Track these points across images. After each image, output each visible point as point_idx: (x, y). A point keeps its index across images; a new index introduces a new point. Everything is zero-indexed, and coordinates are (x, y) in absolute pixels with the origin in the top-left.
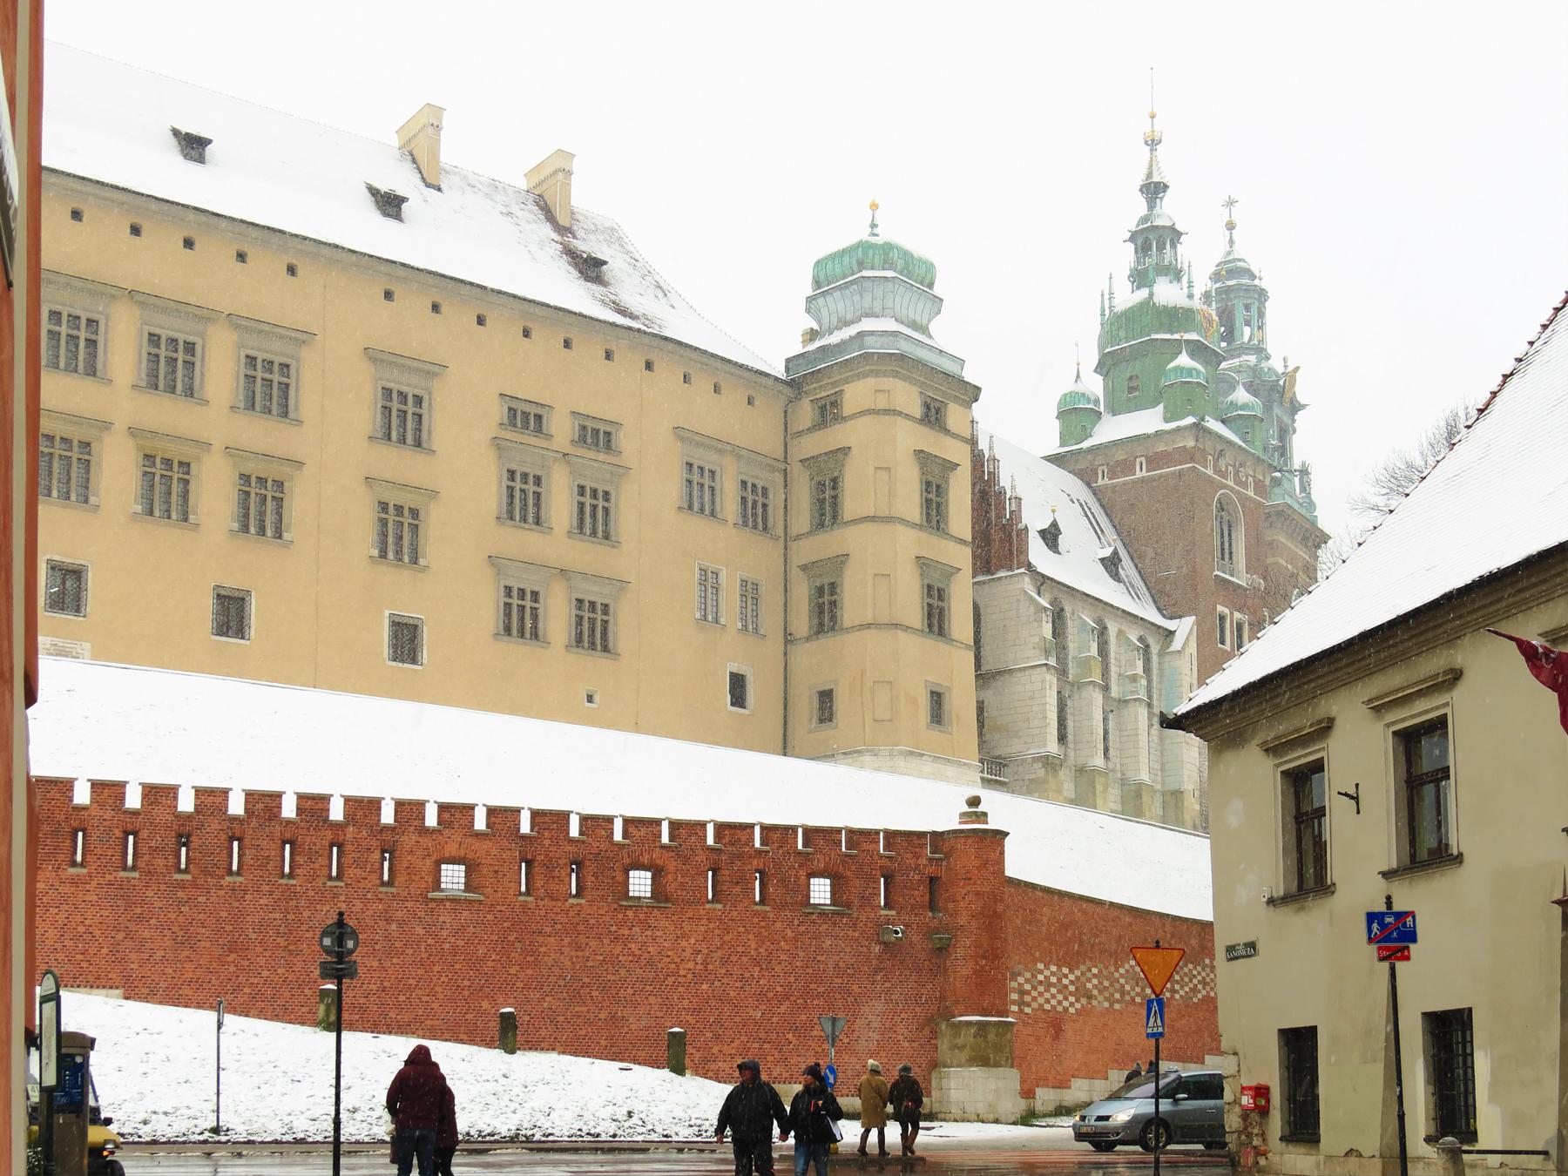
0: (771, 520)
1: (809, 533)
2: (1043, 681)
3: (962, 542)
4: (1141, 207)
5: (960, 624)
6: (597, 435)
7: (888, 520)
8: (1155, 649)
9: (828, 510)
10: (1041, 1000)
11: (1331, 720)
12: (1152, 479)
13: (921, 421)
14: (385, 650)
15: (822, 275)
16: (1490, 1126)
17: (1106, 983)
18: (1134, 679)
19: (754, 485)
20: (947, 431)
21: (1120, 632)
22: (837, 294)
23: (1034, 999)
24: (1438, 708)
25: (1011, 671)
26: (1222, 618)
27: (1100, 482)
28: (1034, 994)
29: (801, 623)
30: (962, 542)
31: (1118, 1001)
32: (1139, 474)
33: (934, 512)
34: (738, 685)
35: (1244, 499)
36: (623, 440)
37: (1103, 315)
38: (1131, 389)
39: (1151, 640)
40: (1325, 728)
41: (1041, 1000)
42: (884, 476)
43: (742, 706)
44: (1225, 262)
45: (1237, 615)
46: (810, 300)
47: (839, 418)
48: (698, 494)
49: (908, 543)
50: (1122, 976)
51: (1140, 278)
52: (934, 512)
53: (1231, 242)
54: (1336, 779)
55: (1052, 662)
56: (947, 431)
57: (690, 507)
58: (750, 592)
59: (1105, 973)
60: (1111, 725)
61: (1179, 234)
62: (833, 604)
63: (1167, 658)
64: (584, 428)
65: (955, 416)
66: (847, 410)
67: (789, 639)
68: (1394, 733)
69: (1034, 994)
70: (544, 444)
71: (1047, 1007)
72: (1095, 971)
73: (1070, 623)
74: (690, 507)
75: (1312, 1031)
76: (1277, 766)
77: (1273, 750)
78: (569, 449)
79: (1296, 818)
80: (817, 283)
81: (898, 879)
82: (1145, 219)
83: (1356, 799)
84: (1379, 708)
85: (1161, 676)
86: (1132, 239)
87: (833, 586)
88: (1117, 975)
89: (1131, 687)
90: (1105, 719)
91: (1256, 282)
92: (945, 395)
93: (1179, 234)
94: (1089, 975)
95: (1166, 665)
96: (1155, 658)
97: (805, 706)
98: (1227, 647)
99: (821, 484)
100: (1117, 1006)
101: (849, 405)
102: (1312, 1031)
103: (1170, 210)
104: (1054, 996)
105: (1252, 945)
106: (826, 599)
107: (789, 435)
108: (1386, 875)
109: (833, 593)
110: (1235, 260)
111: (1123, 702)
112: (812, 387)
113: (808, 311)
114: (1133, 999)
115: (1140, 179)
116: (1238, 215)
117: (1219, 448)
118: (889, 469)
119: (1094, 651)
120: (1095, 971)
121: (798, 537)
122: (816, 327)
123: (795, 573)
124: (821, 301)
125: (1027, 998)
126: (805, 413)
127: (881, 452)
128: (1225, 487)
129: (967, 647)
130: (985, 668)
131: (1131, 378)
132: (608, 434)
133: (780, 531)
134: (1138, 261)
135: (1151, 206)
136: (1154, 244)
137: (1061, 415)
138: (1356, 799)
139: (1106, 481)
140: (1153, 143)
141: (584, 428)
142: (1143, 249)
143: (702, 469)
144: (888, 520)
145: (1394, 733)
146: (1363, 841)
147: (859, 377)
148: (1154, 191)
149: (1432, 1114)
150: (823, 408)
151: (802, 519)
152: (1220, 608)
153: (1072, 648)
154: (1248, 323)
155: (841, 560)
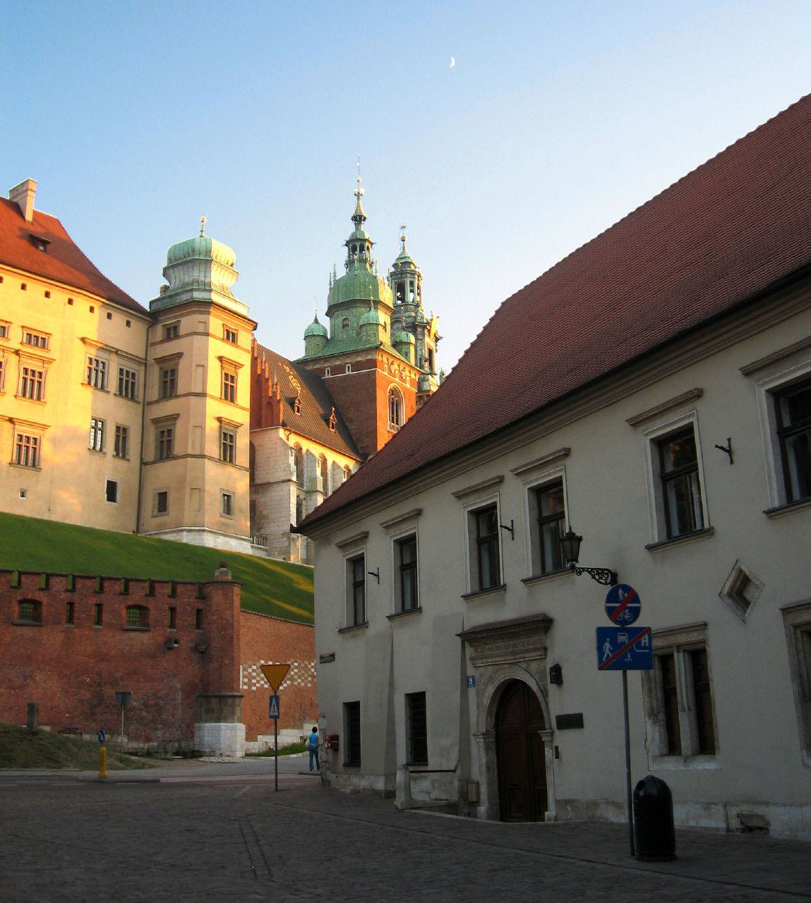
0: (136, 393)
1: (157, 402)
3: (243, 409)
5: (242, 457)
6: (37, 339)
9: (169, 387)
11: (368, 533)
12: (354, 376)
14: (325, 313)
15: (172, 254)
16: (433, 761)
19: (127, 372)
20: (238, 347)
22: (180, 267)
24: (411, 529)
25: (269, 484)
27: (327, 376)
29: (151, 455)
30: (243, 409)
32: (347, 373)
34: (112, 489)
35: (404, 388)
36: (53, 343)
37: (330, 284)
40: (365, 537)
42: (201, 368)
43: (114, 501)
44: (401, 259)
46: (165, 269)
47: (177, 337)
48: (96, 376)
50: (313, 667)
51: (350, 264)
53: (404, 248)
54: (370, 565)
57: (89, 383)
58: (122, 432)
59: (302, 665)
62: (169, 441)
64: (29, 335)
66: (182, 331)
67: (143, 463)
68: (395, 541)
70: (6, 344)
72: (296, 664)
74: (89, 383)
75: (358, 703)
76: (344, 556)
77: (343, 546)
78: (18, 347)
79: (354, 585)
80: (170, 260)
81: (178, 610)
82: (353, 234)
83: (377, 576)
84: (387, 527)
87: (169, 431)
88: (309, 666)
91: (417, 270)
97: (150, 502)
99: (166, 372)
101: (183, 330)
102: (358, 703)
103: (367, 230)
105: (333, 655)
106: (165, 439)
107: (149, 345)
108: (390, 618)
109: (169, 435)
110: (405, 258)
113: (164, 275)
115: (353, 213)
116: (406, 233)
117: (390, 360)
118: (203, 366)
120: (296, 664)
122: (168, 284)
123: (148, 421)
124: (171, 271)
126: (159, 331)
128: (394, 382)
130: (258, 481)
131: (344, 320)
132: (44, 339)
133: (141, 399)
134: (349, 257)
138: (377, 576)
141: (29, 335)
142: (353, 249)
143: (97, 361)
145: (395, 541)
146: (382, 596)
147: (189, 314)
148: (358, 219)
149: (716, 742)
150: (169, 330)
151: (154, 393)
154: (412, 291)
155: (174, 418)
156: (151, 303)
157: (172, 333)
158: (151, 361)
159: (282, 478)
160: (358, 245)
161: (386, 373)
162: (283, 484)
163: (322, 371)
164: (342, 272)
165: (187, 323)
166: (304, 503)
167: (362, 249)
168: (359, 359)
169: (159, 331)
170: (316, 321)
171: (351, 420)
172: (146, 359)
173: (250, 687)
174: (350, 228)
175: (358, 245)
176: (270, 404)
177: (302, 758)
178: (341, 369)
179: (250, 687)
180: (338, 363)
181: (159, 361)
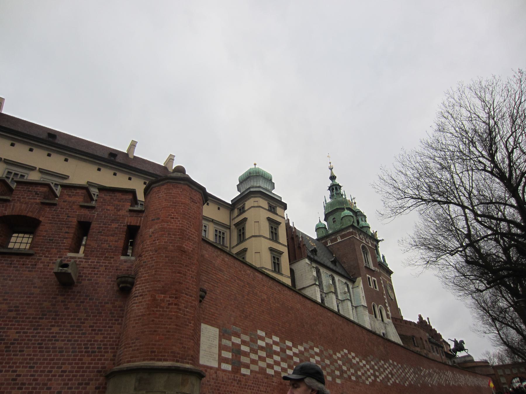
2: (315, 289)
4: (331, 182)
7: (260, 236)
8: (351, 286)
10: (262, 364)
13: (268, 210)
17: (327, 362)
18: (345, 293)
21: (339, 280)
23: (254, 362)
26: (369, 278)
27: (329, 245)
28: (253, 356)
31: (338, 377)
32: (339, 241)
33: (274, 236)
38: (334, 222)
39: (348, 283)
41: (262, 364)
42: (257, 224)
45: (373, 278)
46: (238, 186)
47: (244, 211)
49: (267, 244)
51: (332, 197)
52: (274, 236)
55: (317, 283)
56: (277, 214)
60: (340, 308)
61: (341, 187)
63: (355, 289)
65: (279, 210)
69: (253, 356)
71: (270, 372)
72: (317, 350)
73: (322, 275)
85: (354, 295)
86: (329, 189)
88: (335, 357)
89: (345, 296)
90: (338, 306)
92: (277, 204)
93: (341, 187)
94: (311, 352)
95: (355, 291)
96: (351, 289)
98: (372, 287)
99: (240, 230)
100: (338, 381)
103: (337, 181)
104: (277, 363)
111: (343, 301)
112: (238, 204)
114: (350, 377)
115: (329, 176)
119: (331, 282)
120: (317, 350)
121: (233, 247)
124: (241, 186)
125: (244, 360)
127: (257, 216)
129: (288, 277)
131: (334, 219)
133: (228, 245)
135: (332, 173)
136: (335, 188)
137: (316, 230)
139: (330, 244)
140: (331, 169)
144: (260, 236)
148: (333, 178)
150: (240, 210)
152: (367, 275)
153: (324, 283)
156: (232, 201)
157: (242, 211)
158: (233, 227)
159: (311, 284)
160: (334, 187)
161: (358, 238)
162: (311, 287)
163: (326, 243)
164: (329, 200)
165: (249, 203)
166: (325, 299)
167: (336, 189)
168: (344, 233)
169: (236, 212)
170: (320, 221)
171: (345, 263)
172: (230, 226)
173: (236, 370)
174: (330, 182)
175: (334, 187)
176: (299, 247)
177: (457, 165)
178: (336, 239)
179: (236, 370)
180: (333, 237)
181: (237, 225)
